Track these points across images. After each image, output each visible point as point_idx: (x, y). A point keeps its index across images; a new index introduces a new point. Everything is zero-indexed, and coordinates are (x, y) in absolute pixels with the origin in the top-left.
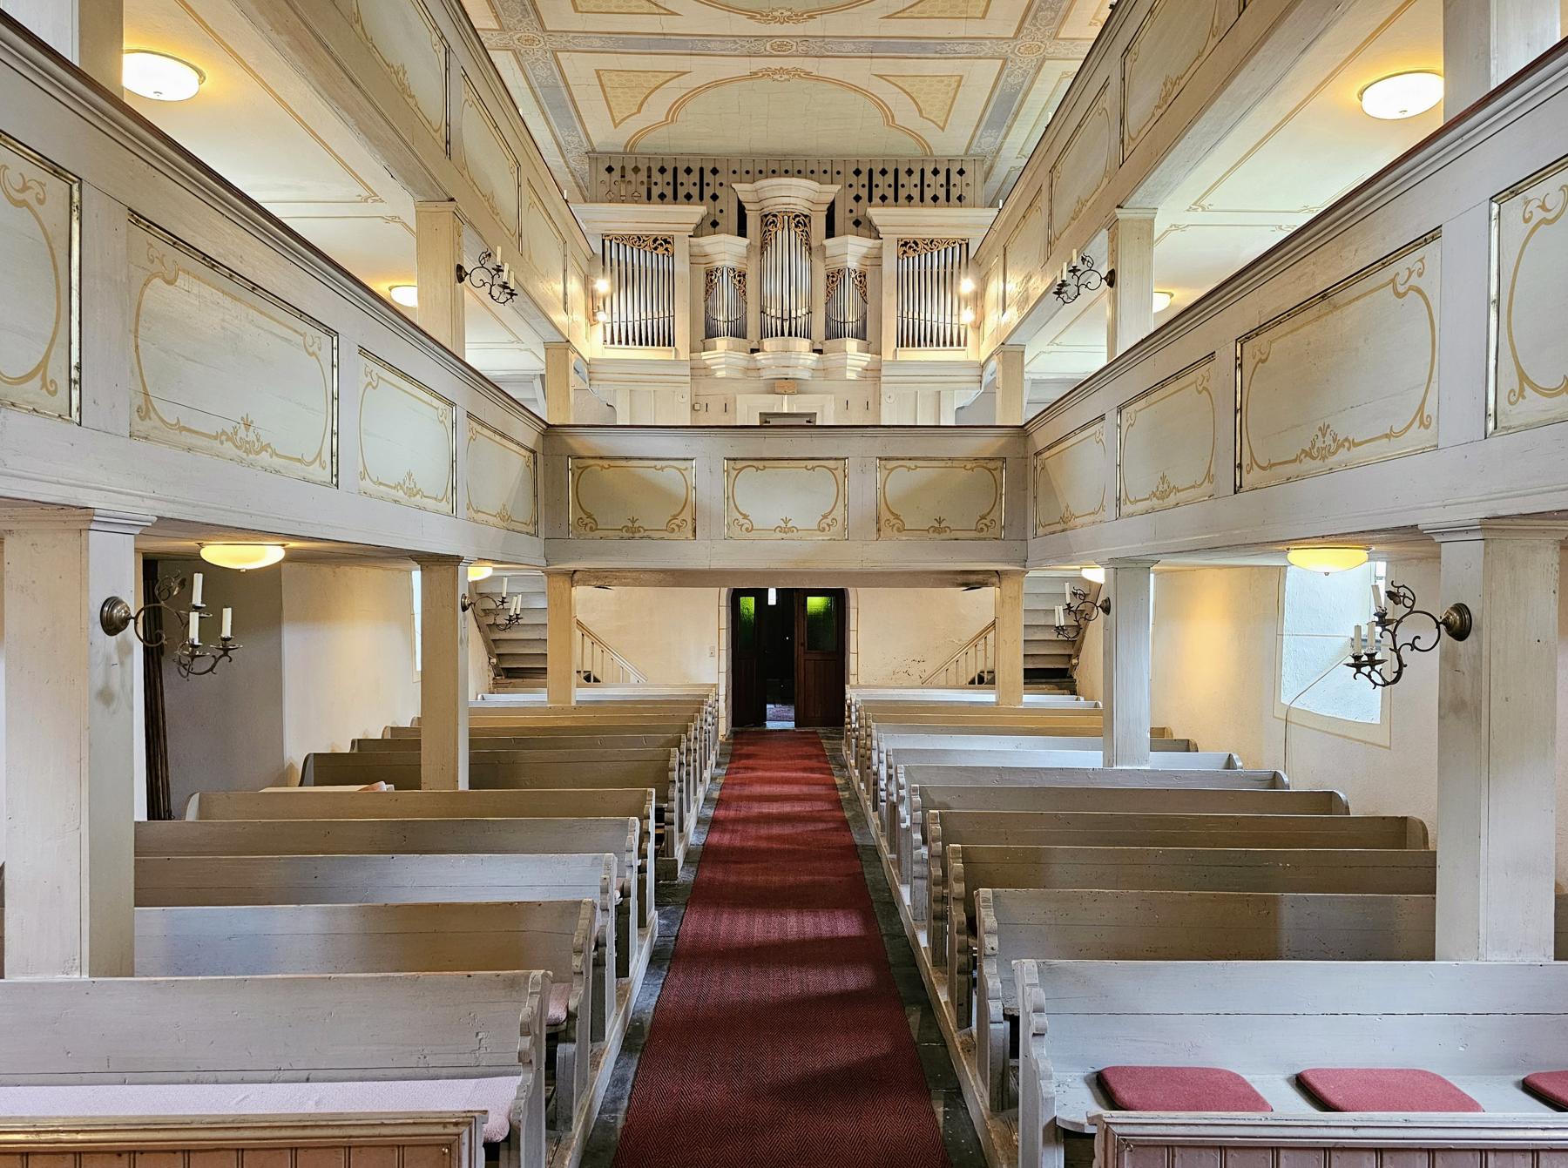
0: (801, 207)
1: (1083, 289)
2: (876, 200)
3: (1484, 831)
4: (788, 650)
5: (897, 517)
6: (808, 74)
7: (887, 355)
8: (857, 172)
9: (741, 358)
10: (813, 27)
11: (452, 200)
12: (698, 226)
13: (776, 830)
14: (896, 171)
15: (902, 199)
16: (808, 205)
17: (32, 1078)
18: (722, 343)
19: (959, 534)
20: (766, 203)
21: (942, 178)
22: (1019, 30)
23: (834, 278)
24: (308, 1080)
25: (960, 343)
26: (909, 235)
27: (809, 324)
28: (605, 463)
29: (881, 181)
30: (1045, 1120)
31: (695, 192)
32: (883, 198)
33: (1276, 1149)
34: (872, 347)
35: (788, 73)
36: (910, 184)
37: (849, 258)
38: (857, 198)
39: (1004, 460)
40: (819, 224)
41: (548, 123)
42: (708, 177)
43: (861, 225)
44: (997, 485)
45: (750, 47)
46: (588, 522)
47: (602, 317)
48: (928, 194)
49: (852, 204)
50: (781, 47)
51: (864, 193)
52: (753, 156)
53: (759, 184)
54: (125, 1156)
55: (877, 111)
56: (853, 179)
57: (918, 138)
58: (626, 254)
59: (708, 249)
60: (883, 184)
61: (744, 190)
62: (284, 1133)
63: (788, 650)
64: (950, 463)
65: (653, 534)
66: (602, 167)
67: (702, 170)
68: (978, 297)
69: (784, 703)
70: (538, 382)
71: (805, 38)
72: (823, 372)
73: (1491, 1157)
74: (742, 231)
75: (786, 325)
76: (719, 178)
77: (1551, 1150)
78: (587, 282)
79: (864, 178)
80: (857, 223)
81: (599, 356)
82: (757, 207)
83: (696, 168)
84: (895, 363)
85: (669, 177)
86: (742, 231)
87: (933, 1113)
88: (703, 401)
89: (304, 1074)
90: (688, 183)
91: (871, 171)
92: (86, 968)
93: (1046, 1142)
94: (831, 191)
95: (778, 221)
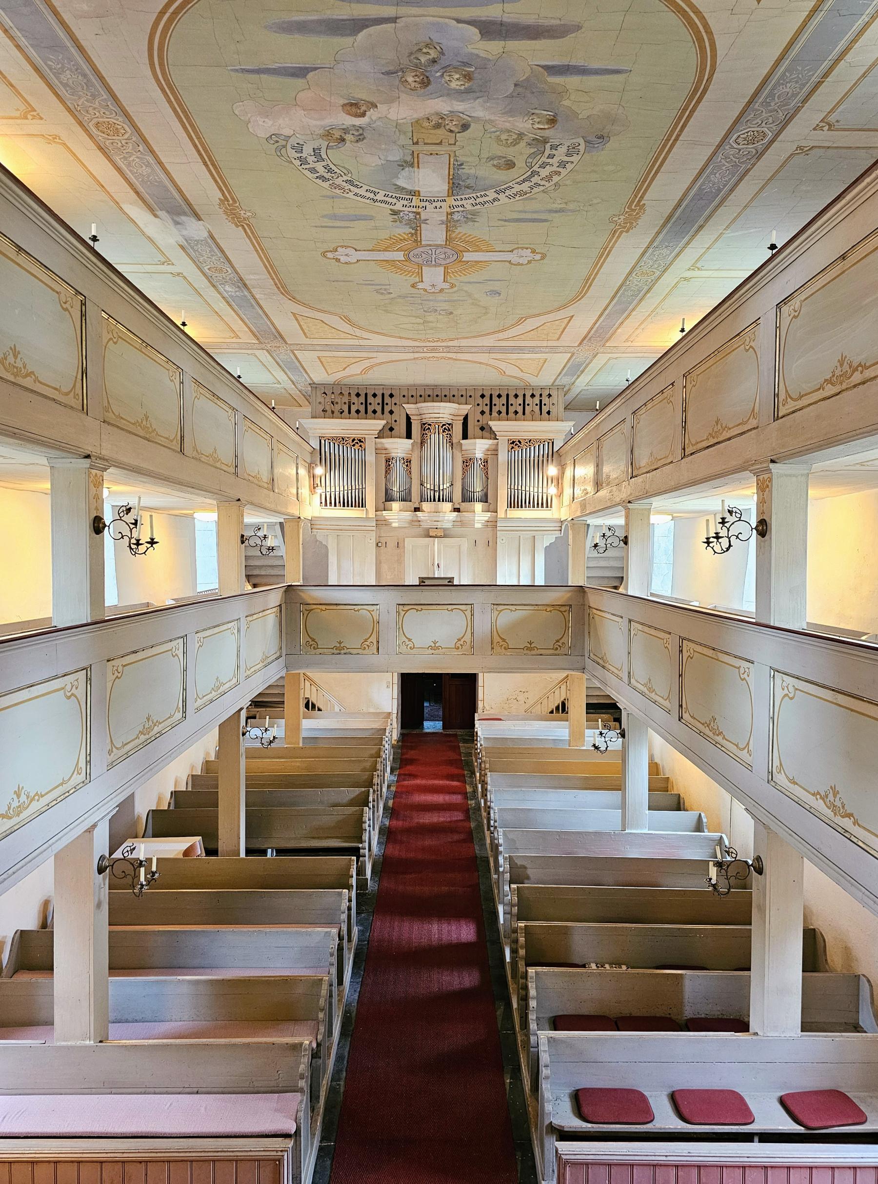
2: (495, 414)
3: (766, 973)
4: (439, 702)
5: (504, 640)
7: (501, 514)
8: (483, 396)
9: (408, 515)
10: (455, 343)
11: (239, 500)
13: (428, 842)
14: (508, 395)
15: (511, 414)
16: (451, 417)
17: (68, 1091)
18: (395, 505)
19: (543, 652)
20: (424, 416)
22: (580, 344)
23: (467, 463)
24: (197, 1093)
25: (546, 504)
26: (516, 437)
27: (452, 493)
28: (323, 607)
30: (547, 1122)
31: (379, 409)
33: (632, 1165)
38: (483, 413)
39: (570, 606)
41: (286, 374)
42: (387, 399)
43: (486, 431)
44: (566, 622)
45: (414, 350)
46: (313, 644)
49: (479, 417)
52: (416, 387)
53: (419, 405)
54: (143, 1164)
56: (480, 401)
57: (521, 379)
58: (336, 450)
59: (387, 446)
60: (499, 403)
61: (410, 408)
62: (209, 1154)
63: (439, 702)
64: (536, 608)
65: (352, 651)
67: (383, 395)
68: (558, 481)
69: (436, 702)
70: (278, 527)
72: (461, 523)
73: (724, 1169)
74: (409, 436)
75: (437, 495)
76: (394, 400)
77: (750, 1166)
78: (310, 468)
79: (487, 400)
80: (482, 429)
81: (317, 514)
82: (419, 418)
85: (362, 399)
86: (409, 436)
87: (504, 1084)
88: (383, 540)
89: (196, 1090)
90: (375, 404)
92: (92, 1038)
93: (547, 1133)
94: (465, 409)
95: (432, 428)
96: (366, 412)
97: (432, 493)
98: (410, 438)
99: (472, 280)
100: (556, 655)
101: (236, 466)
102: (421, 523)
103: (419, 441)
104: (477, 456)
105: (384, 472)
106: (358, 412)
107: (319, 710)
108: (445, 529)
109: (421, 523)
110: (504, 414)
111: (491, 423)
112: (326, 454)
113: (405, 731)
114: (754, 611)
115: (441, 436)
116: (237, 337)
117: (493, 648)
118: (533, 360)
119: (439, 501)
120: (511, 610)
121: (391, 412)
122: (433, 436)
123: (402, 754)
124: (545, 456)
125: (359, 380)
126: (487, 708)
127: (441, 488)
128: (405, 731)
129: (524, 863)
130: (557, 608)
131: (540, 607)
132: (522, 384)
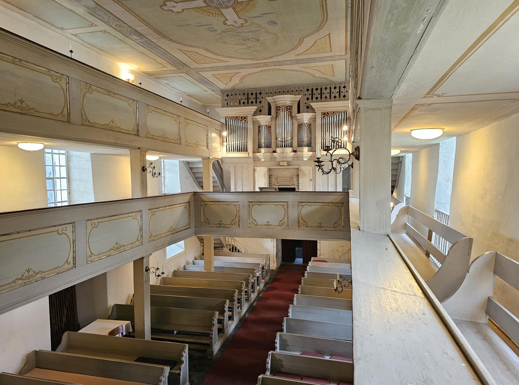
0: (288, 103)
2: (314, 99)
5: (305, 222)
12: (255, 112)
15: (323, 99)
18: (263, 150)
23: (300, 126)
26: (325, 111)
28: (212, 203)
29: (317, 92)
31: (254, 101)
34: (313, 149)
36: (326, 92)
38: (308, 99)
39: (343, 203)
40: (295, 109)
42: (258, 96)
45: (257, 66)
46: (208, 222)
47: (225, 144)
48: (333, 95)
49: (306, 101)
50: (266, 65)
51: (310, 97)
52: (272, 88)
56: (306, 92)
57: (326, 79)
58: (231, 123)
59: (258, 120)
60: (317, 93)
61: (270, 99)
64: (323, 204)
66: (225, 95)
71: (273, 62)
79: (310, 92)
80: (308, 107)
81: (225, 156)
83: (254, 93)
86: (270, 114)
90: (252, 98)
91: (312, 89)
96: (248, 103)
98: (270, 115)
99: (255, 15)
101: (138, 131)
104: (305, 122)
106: (244, 103)
107: (239, 251)
108: (288, 162)
110: (319, 99)
111: (312, 104)
113: (283, 263)
116: (164, 67)
117: (299, 226)
118: (326, 66)
119: (285, 147)
123: (276, 276)
124: (343, 120)
125: (241, 86)
126: (322, 254)
128: (283, 263)
129: (281, 358)
130: (335, 204)
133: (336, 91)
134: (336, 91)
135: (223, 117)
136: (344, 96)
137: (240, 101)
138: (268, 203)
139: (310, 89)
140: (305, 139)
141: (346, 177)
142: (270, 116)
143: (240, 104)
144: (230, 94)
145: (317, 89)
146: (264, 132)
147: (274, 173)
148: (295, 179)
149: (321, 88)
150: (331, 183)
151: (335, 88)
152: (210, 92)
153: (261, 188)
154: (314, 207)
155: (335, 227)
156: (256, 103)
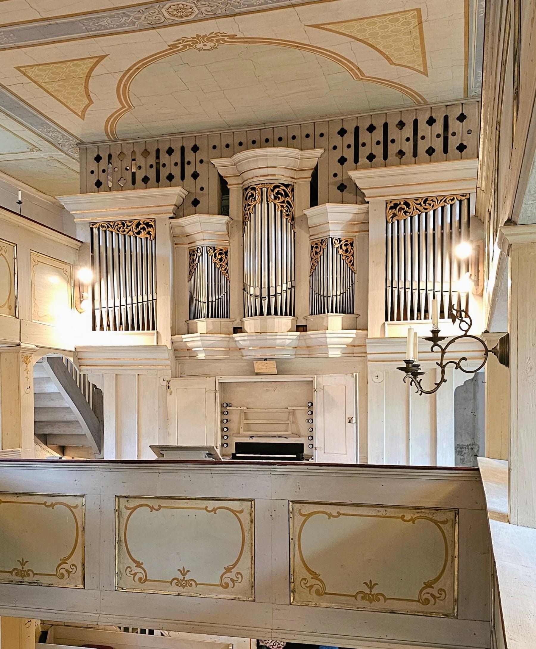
0: (282, 176)
1: (450, 369)
2: (363, 160)
5: (315, 576)
6: (232, 37)
7: (374, 332)
12: (177, 207)
20: (245, 176)
21: (438, 127)
23: (318, 247)
26: (399, 195)
31: (176, 172)
32: (371, 157)
35: (209, 39)
36: (401, 138)
37: (331, 227)
38: (342, 160)
39: (457, 512)
40: (303, 192)
42: (189, 156)
43: (347, 190)
44: (448, 545)
48: (423, 146)
49: (337, 168)
51: (349, 154)
52: (230, 128)
53: (239, 156)
55: (336, 66)
56: (338, 140)
59: (189, 230)
60: (371, 142)
61: (223, 165)
76: (199, 155)
79: (350, 138)
80: (342, 188)
84: (383, 340)
86: (224, 210)
91: (357, 129)
97: (258, 301)
100: (424, 614)
102: (244, 353)
103: (241, 219)
104: (332, 234)
105: (187, 273)
106: (146, 180)
109: (244, 353)
110: (379, 158)
111: (353, 174)
112: (118, 249)
114: (490, 521)
115: (272, 205)
117: (292, 591)
119: (269, 313)
120: (330, 515)
121: (195, 175)
122: (258, 206)
124: (455, 224)
127: (272, 292)
131: (391, 512)
132: (409, 101)
133: (437, 132)
134: (437, 132)
135: (83, 224)
136: (461, 148)
137: (134, 174)
138: (182, 503)
139: (350, 128)
140: (334, 290)
141: (468, 412)
142: (225, 218)
143: (134, 183)
144: (105, 156)
145: (371, 129)
146: (205, 265)
147: (238, 397)
148: (302, 416)
149: (386, 126)
150: (415, 436)
151: (431, 121)
152: (47, 151)
153: (159, 449)
154: (350, 524)
155: (427, 601)
156: (183, 178)
